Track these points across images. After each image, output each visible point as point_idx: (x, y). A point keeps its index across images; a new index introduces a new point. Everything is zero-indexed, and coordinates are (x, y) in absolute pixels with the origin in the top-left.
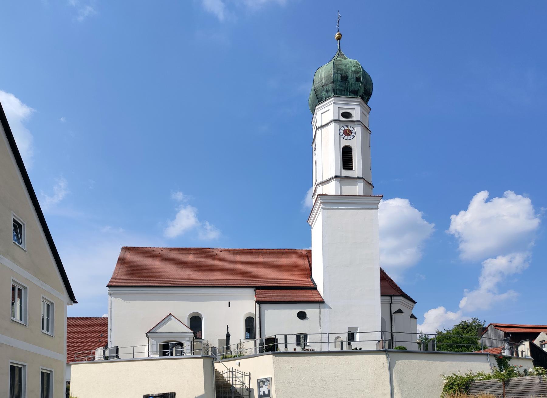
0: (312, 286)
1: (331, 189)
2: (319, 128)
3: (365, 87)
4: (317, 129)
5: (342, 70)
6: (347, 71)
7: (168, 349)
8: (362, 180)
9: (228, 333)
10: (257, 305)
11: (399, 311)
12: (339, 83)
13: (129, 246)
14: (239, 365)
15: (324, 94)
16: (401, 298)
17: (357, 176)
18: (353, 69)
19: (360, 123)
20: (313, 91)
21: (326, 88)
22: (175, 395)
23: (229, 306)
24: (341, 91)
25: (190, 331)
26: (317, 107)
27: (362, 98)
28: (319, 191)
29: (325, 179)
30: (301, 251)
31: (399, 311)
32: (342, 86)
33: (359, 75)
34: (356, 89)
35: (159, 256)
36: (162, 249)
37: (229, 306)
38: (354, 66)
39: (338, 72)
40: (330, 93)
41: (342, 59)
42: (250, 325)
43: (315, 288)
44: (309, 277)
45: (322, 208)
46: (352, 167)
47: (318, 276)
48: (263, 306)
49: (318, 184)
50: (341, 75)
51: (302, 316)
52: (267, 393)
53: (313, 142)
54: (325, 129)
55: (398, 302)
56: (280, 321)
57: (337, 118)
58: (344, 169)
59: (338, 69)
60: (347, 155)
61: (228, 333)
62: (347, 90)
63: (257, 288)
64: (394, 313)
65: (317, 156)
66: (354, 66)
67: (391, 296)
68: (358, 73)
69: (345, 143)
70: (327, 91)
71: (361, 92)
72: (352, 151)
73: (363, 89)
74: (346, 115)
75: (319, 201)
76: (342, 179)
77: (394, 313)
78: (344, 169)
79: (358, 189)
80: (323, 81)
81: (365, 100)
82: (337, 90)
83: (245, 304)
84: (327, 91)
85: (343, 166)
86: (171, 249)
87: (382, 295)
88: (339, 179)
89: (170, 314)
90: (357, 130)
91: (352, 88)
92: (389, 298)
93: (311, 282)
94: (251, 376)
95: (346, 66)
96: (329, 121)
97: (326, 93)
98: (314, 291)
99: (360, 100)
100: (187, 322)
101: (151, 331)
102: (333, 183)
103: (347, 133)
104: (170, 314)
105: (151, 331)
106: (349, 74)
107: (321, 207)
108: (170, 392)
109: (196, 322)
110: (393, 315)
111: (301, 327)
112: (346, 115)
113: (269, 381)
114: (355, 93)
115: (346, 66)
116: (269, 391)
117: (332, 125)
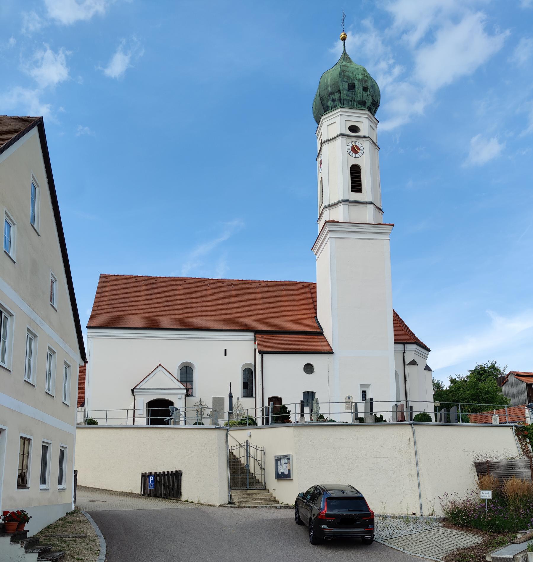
0: (319, 330)
1: (340, 214)
2: (325, 142)
3: (372, 97)
4: (322, 143)
5: (348, 77)
6: (354, 79)
7: (160, 412)
8: (372, 205)
9: (230, 392)
10: (258, 355)
11: (413, 363)
12: (346, 92)
13: (108, 273)
14: (250, 436)
15: (330, 103)
16: (415, 346)
17: (366, 200)
18: (361, 77)
19: (369, 139)
20: (318, 98)
21: (332, 96)
22: (182, 474)
23: (225, 355)
24: (348, 101)
25: (182, 387)
26: (322, 118)
27: (370, 109)
28: (327, 216)
29: (332, 202)
30: (303, 284)
31: (413, 363)
32: (349, 96)
33: (367, 83)
34: (364, 100)
35: (143, 287)
36: (146, 278)
37: (225, 355)
38: (362, 74)
39: (345, 80)
40: (337, 103)
41: (348, 64)
42: (249, 375)
43: (321, 333)
44: (313, 318)
45: (330, 237)
46: (361, 189)
47: (325, 316)
48: (265, 356)
49: (325, 207)
50: (348, 84)
51: (309, 369)
52: (286, 472)
53: (318, 156)
54: (331, 144)
55: (412, 351)
56: (283, 378)
57: (344, 133)
58: (352, 191)
59: (344, 76)
60: (355, 173)
61: (230, 392)
62: (354, 101)
63: (256, 332)
64: (409, 364)
65: (323, 172)
66: (362, 74)
67: (404, 343)
68: (366, 81)
69: (353, 162)
70: (334, 100)
71: (368, 104)
72: (360, 171)
73: (370, 99)
74: (354, 129)
75: (327, 229)
76: (351, 204)
77: (409, 364)
78: (352, 191)
79: (368, 215)
80: (329, 89)
81: (373, 112)
82: (344, 99)
83: (241, 348)
84: (334, 100)
85: (352, 188)
86: (156, 279)
87: (395, 343)
88: (348, 203)
89: (160, 365)
90: (365, 145)
91: (359, 98)
92: (401, 346)
93: (316, 325)
94: (266, 451)
95: (353, 73)
96: (336, 135)
97: (332, 103)
98: (320, 337)
99: (368, 112)
100: (177, 374)
101: (138, 387)
102: (342, 207)
103: (355, 150)
104: (160, 365)
105: (138, 387)
106: (356, 82)
107: (329, 236)
108: (175, 470)
109: (186, 373)
110: (406, 366)
111: (309, 383)
112: (354, 129)
113: (289, 459)
114: (363, 103)
115: (353, 73)
116: (289, 471)
117: (340, 140)
